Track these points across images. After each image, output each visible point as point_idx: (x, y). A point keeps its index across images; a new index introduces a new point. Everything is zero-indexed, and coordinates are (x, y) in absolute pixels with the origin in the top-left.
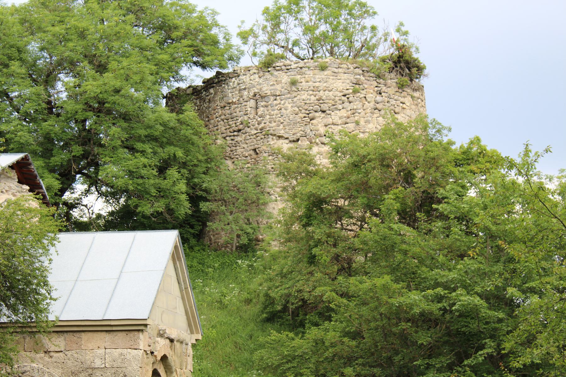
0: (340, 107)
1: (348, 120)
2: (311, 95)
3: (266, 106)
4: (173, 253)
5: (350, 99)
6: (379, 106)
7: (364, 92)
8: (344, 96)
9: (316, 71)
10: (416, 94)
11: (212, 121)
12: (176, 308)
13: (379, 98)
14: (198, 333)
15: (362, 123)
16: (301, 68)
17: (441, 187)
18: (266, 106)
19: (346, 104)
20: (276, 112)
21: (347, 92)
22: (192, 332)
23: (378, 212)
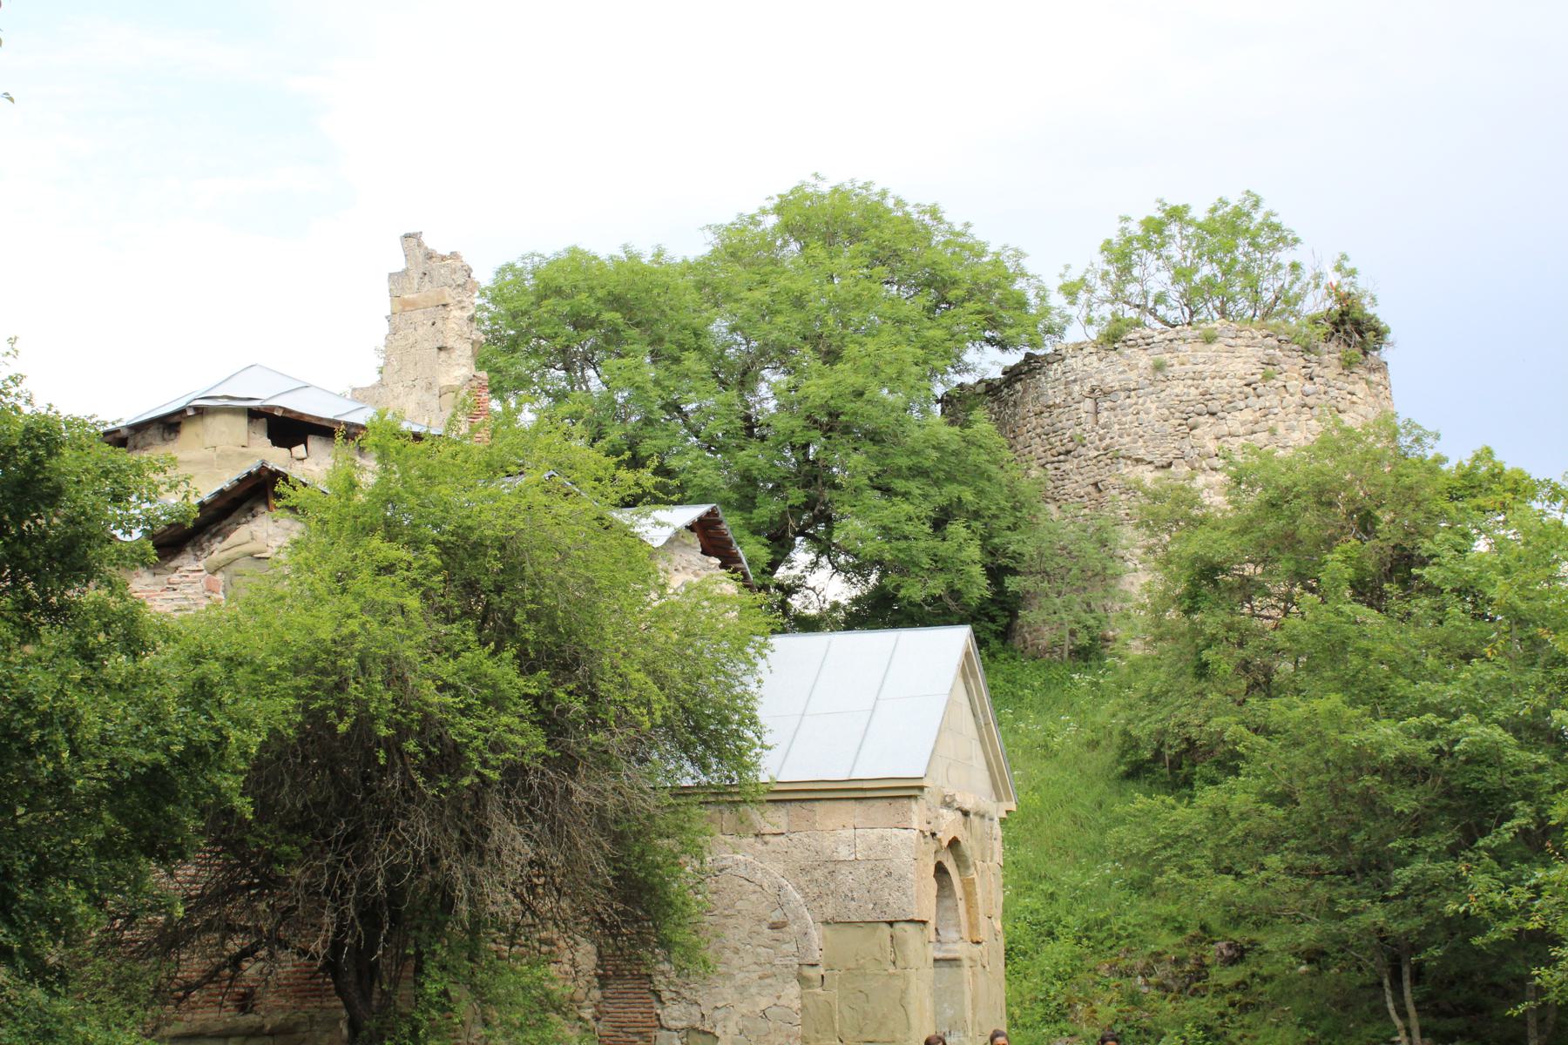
0: (1242, 405)
1: (1256, 428)
3: (1113, 409)
6: (1310, 401)
7: (1282, 377)
10: (1375, 377)
11: (1021, 439)
13: (1309, 387)
14: (1009, 799)
15: (1281, 430)
18: (1113, 409)
19: (1252, 400)
21: (1253, 378)
22: (999, 799)
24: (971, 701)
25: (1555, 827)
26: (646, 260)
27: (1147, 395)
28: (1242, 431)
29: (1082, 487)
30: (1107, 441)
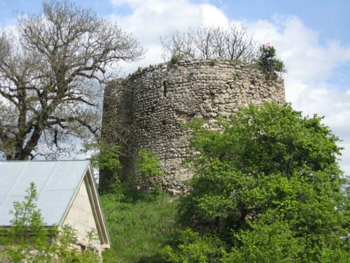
0: (224, 91)
1: (230, 101)
2: (204, 83)
3: (172, 91)
4: (85, 177)
5: (232, 86)
6: (253, 91)
7: (242, 81)
8: (228, 83)
9: (208, 66)
10: (280, 85)
11: (135, 102)
12: (87, 222)
13: (252, 86)
14: (107, 243)
15: (240, 103)
16: (197, 64)
17: (103, 58)
18: (172, 91)
19: (229, 90)
20: (179, 95)
21: (230, 81)
22: (102, 243)
23: (62, 55)
24: (91, 203)
25: (17, 84)
26: (41, 217)
27: (187, 85)
28: (224, 102)
29: (158, 122)
30: (169, 104)
